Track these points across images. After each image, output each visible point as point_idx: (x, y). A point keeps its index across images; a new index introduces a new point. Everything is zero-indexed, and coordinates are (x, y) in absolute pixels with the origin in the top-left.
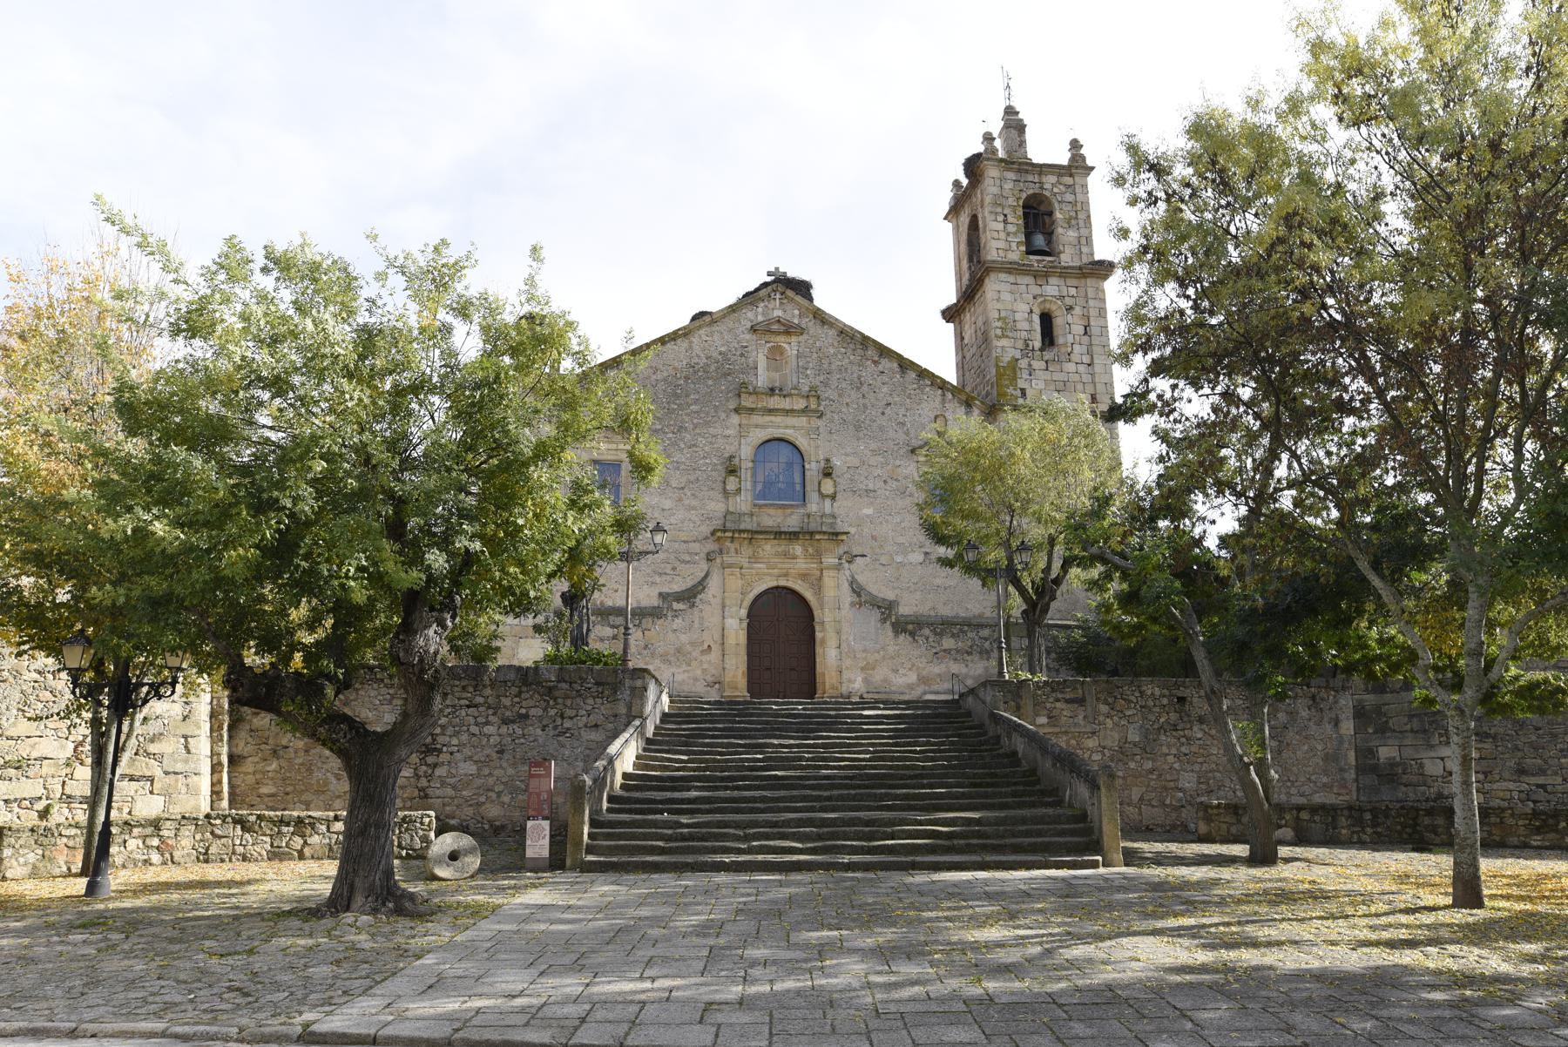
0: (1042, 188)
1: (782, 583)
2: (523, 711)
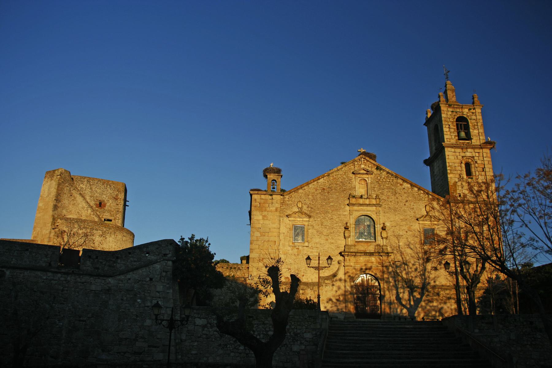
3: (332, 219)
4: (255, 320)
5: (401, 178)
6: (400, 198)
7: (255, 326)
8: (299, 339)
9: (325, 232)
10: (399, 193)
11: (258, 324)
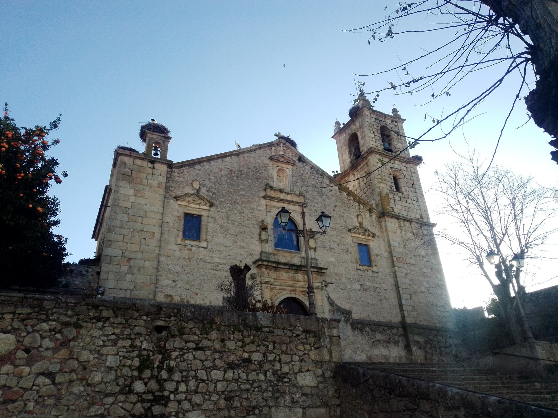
1: (293, 295)
2: (246, 355)
3: (242, 213)
4: (173, 336)
6: (327, 200)
7: (174, 354)
9: (233, 229)
10: (327, 195)
11: (181, 349)
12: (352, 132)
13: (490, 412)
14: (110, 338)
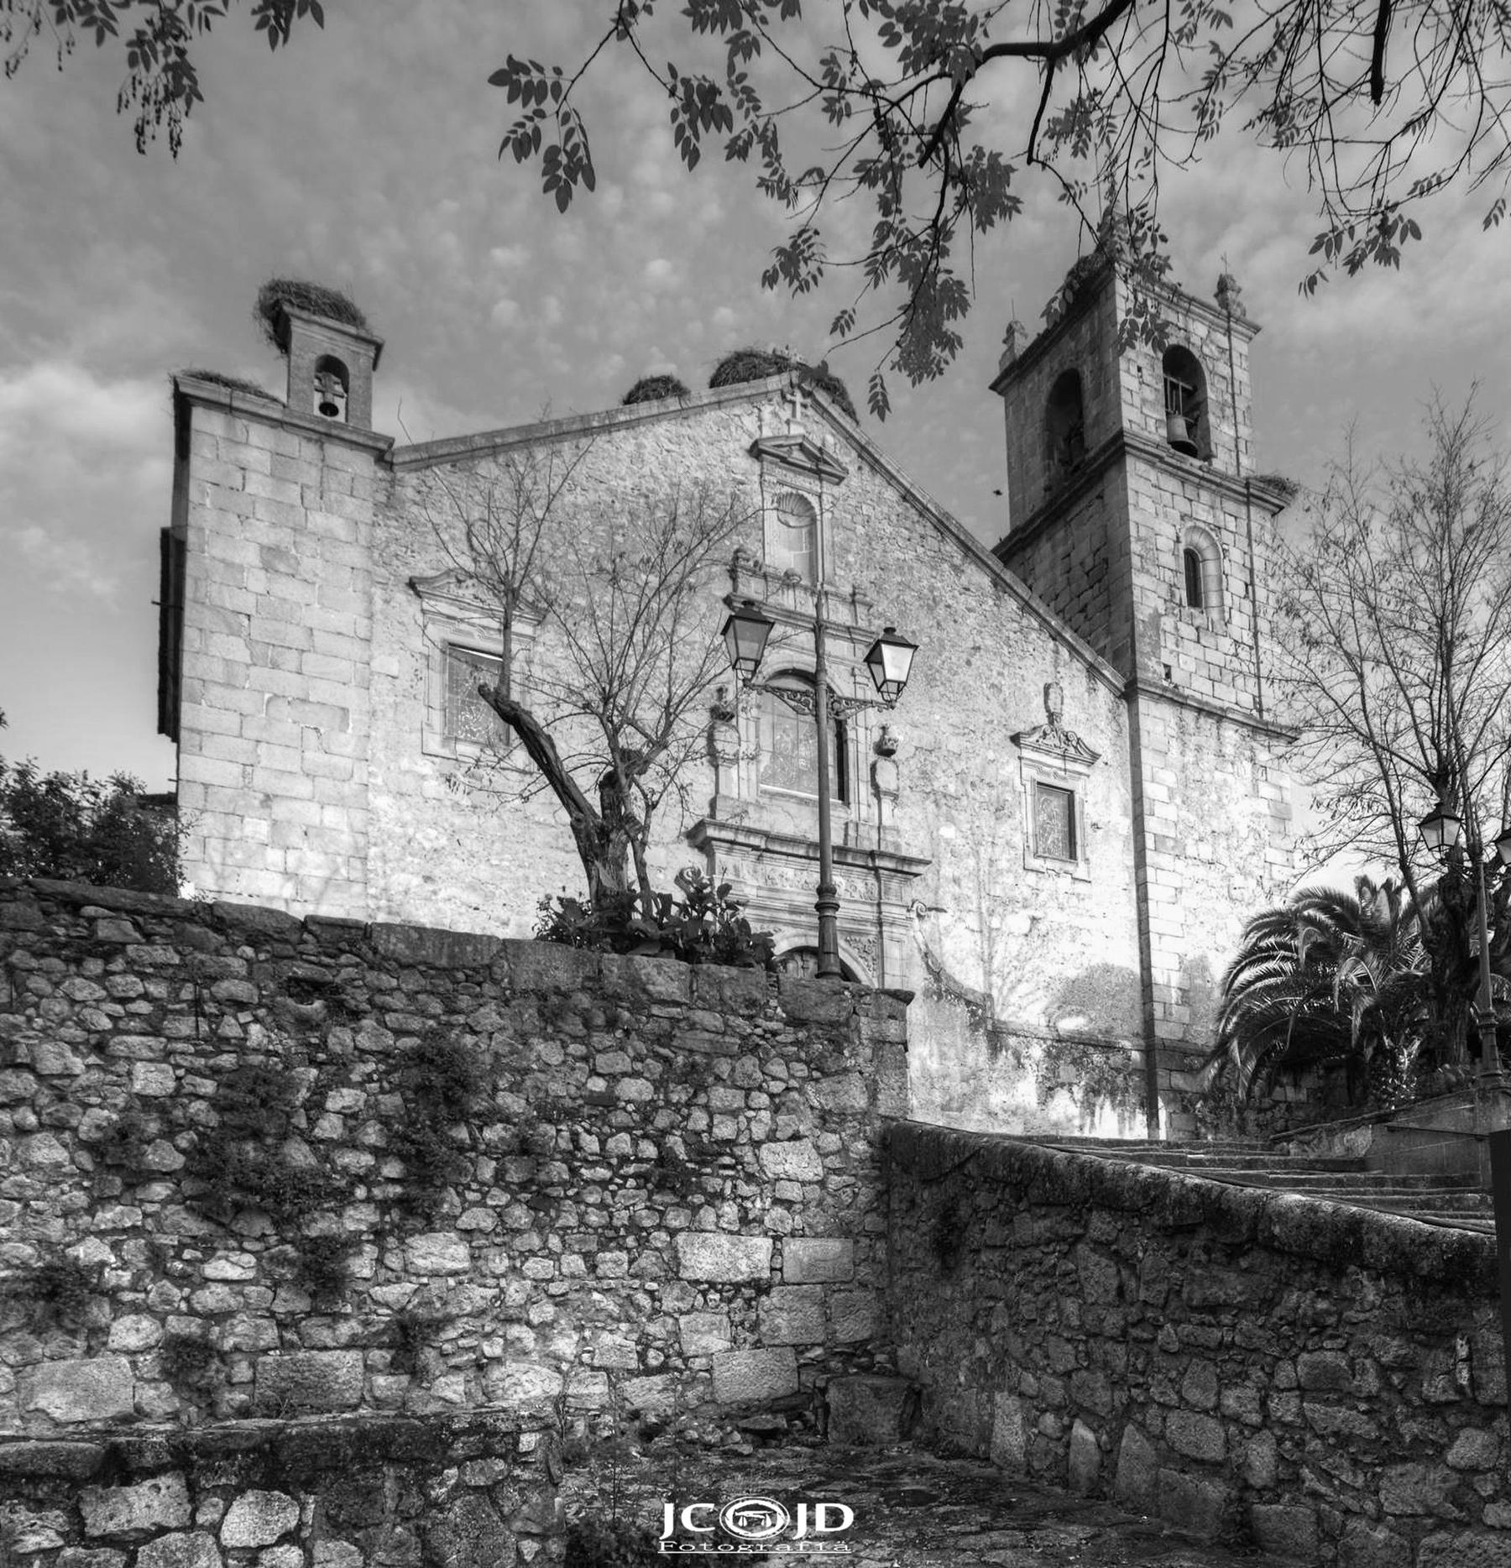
0: (1188, 340)
2: (598, 1085)
5: (957, 538)
8: (729, 1184)
10: (949, 606)
12: (1061, 365)
13: (1273, 1237)
14: (133, 1007)
